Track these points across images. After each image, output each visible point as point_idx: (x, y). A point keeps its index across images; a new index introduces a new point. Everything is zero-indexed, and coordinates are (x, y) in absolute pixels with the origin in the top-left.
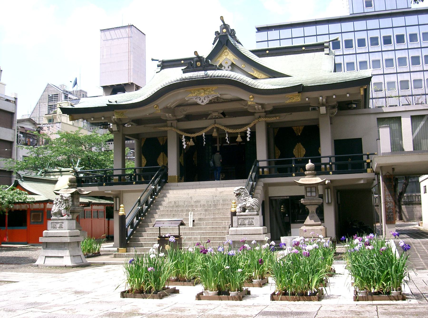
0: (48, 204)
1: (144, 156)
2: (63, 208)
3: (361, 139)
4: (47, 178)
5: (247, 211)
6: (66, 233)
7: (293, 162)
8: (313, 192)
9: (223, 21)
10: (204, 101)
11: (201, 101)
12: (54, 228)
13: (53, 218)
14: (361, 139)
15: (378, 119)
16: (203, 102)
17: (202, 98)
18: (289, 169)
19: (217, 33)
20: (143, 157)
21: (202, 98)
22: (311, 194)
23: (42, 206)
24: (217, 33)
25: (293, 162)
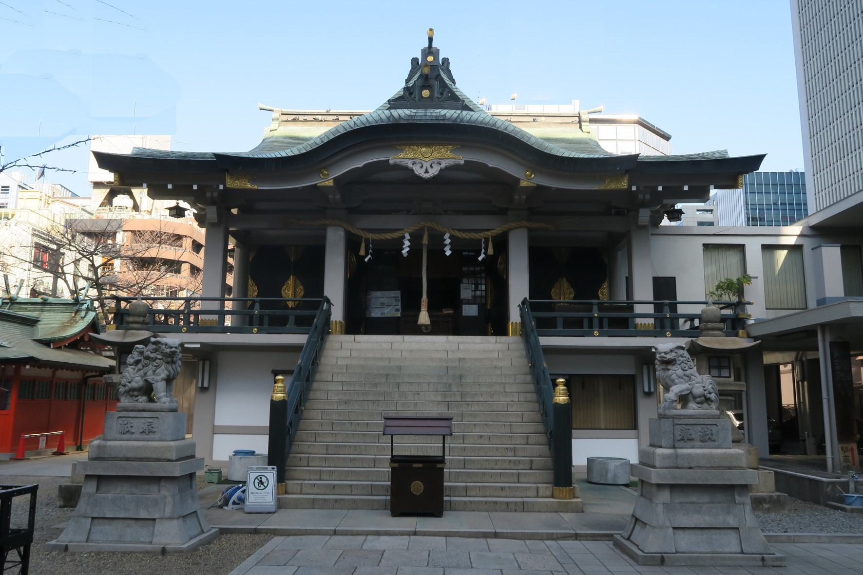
0: (28, 367)
1: (253, 279)
2: (159, 378)
3: (674, 278)
4: (12, 312)
5: (692, 404)
6: (169, 449)
7: (595, 308)
8: (724, 367)
9: (431, 40)
10: (429, 169)
11: (424, 169)
12: (126, 432)
13: (124, 402)
14: (674, 278)
15: (704, 245)
16: (427, 172)
17: (427, 165)
18: (586, 323)
19: (415, 61)
20: (250, 282)
21: (426, 162)
22: (720, 372)
23: (47, 373)
24: (415, 61)
25: (595, 308)
